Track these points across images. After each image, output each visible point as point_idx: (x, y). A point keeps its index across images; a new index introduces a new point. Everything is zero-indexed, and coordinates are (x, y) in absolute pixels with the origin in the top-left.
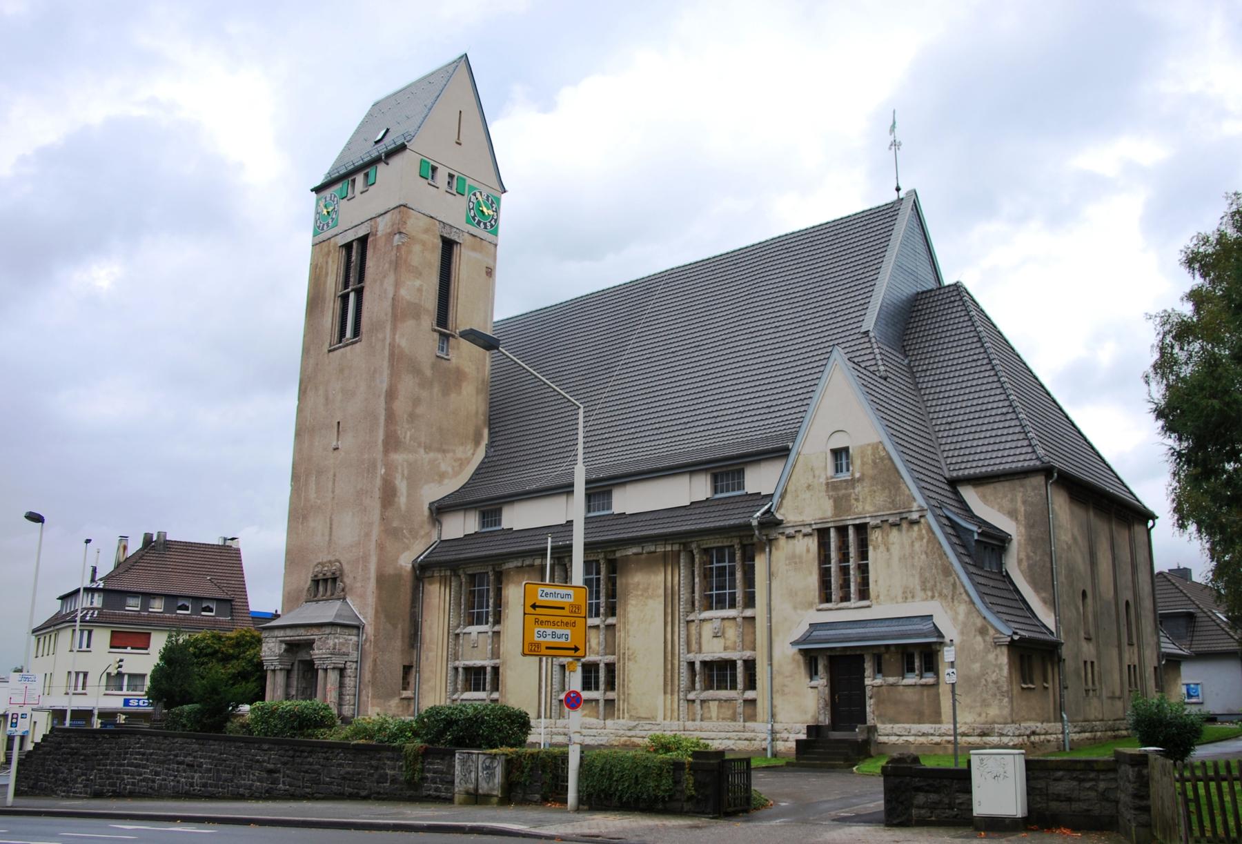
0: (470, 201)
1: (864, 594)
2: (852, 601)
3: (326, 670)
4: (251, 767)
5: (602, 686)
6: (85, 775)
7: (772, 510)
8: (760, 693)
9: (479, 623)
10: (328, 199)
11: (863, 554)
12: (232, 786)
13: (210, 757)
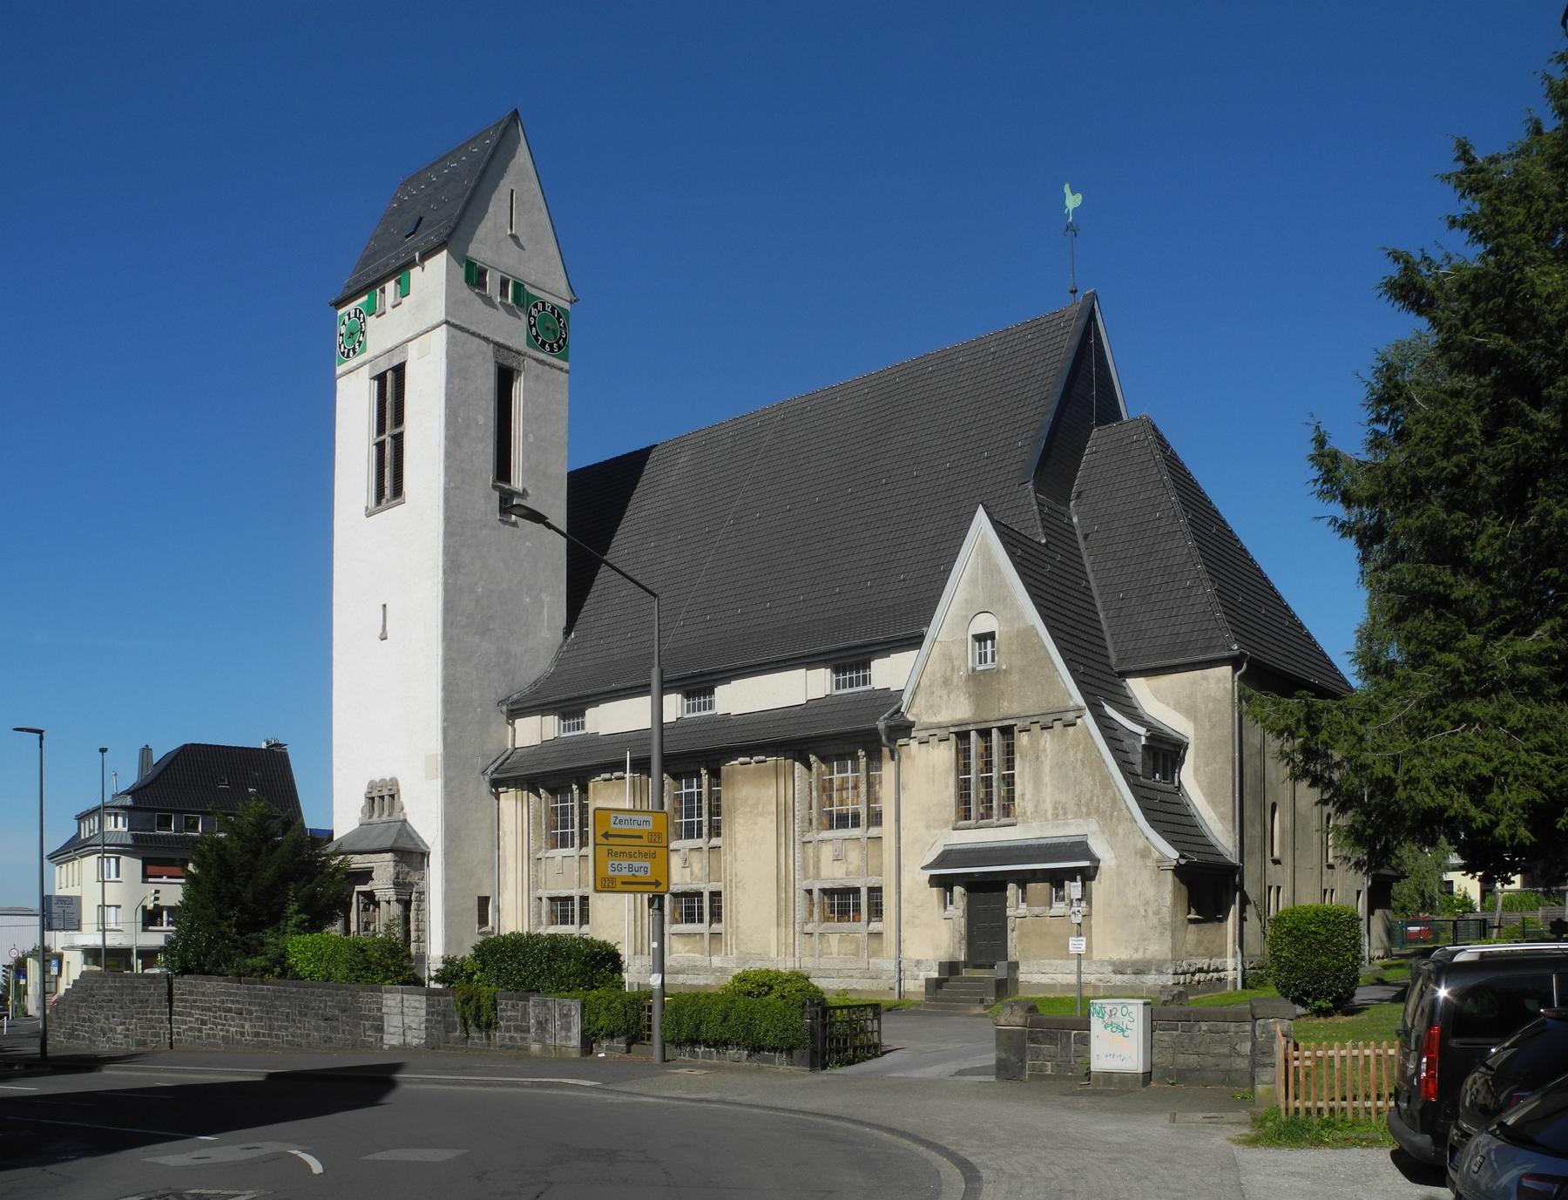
0: (530, 315)
1: (1007, 810)
2: (995, 818)
3: (389, 902)
4: (306, 1015)
5: (706, 917)
6: (124, 1024)
7: (902, 710)
8: (887, 925)
9: (564, 846)
10: (352, 316)
11: (1010, 764)
12: (287, 1036)
13: (260, 1005)
